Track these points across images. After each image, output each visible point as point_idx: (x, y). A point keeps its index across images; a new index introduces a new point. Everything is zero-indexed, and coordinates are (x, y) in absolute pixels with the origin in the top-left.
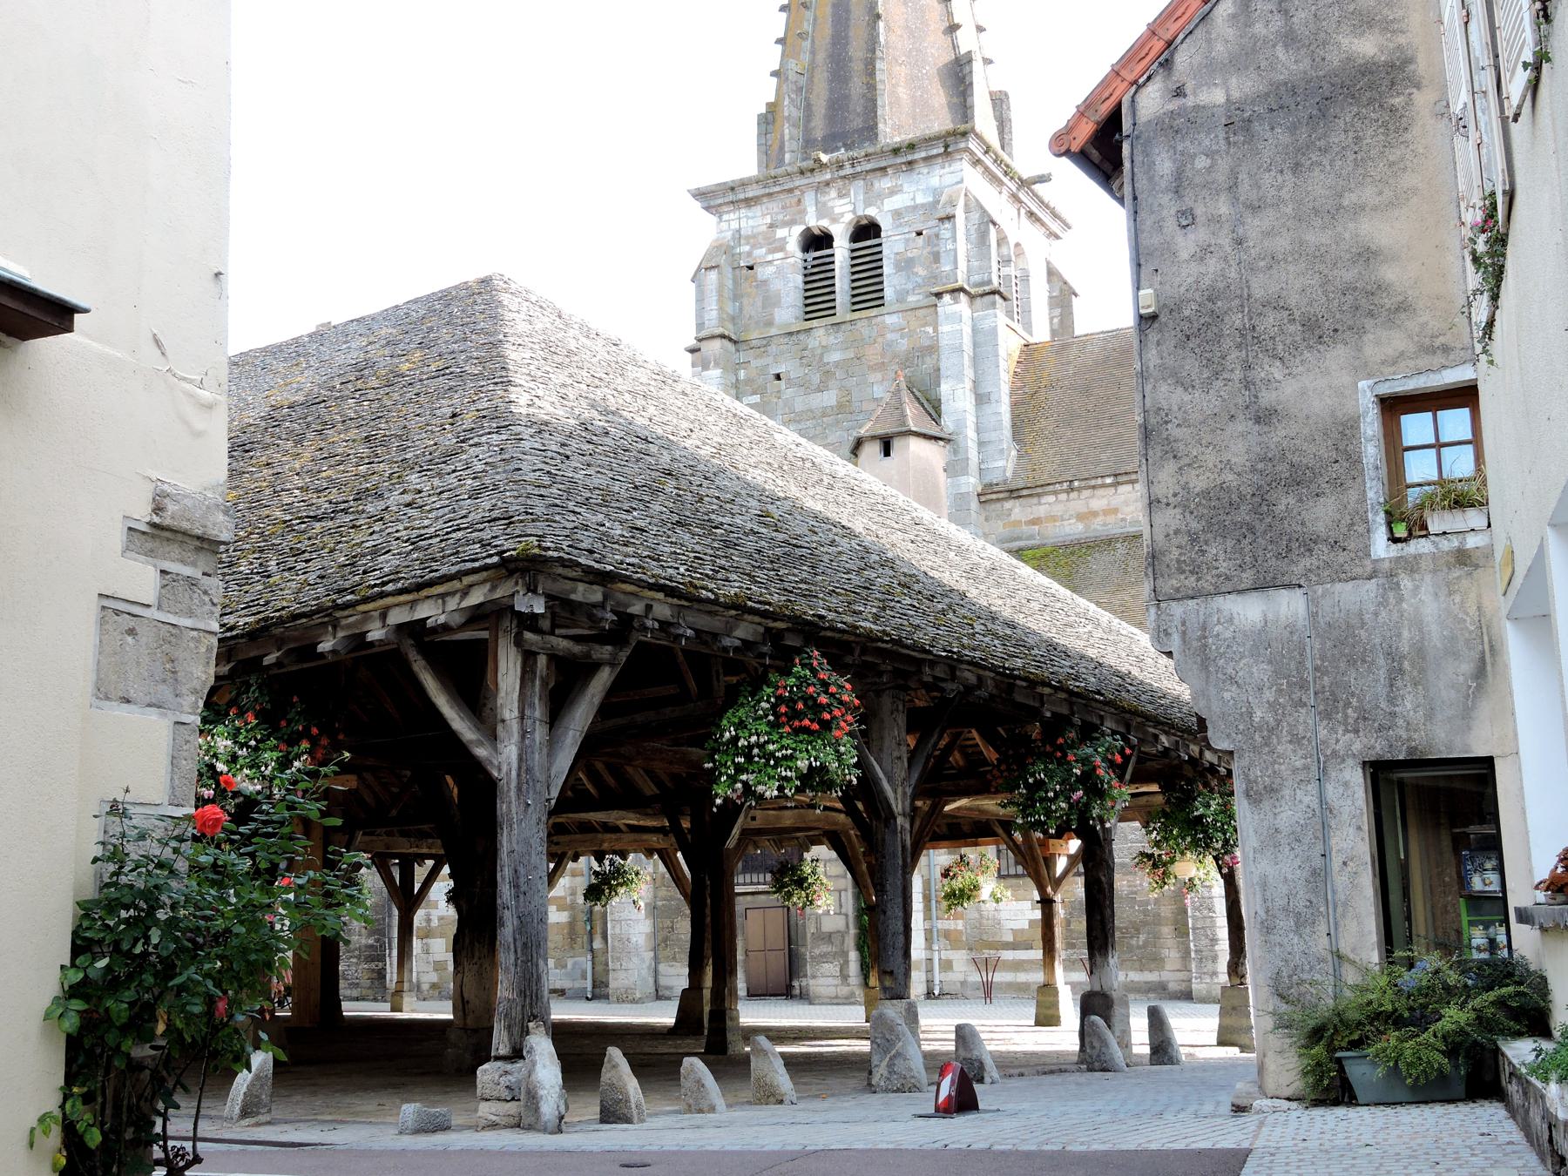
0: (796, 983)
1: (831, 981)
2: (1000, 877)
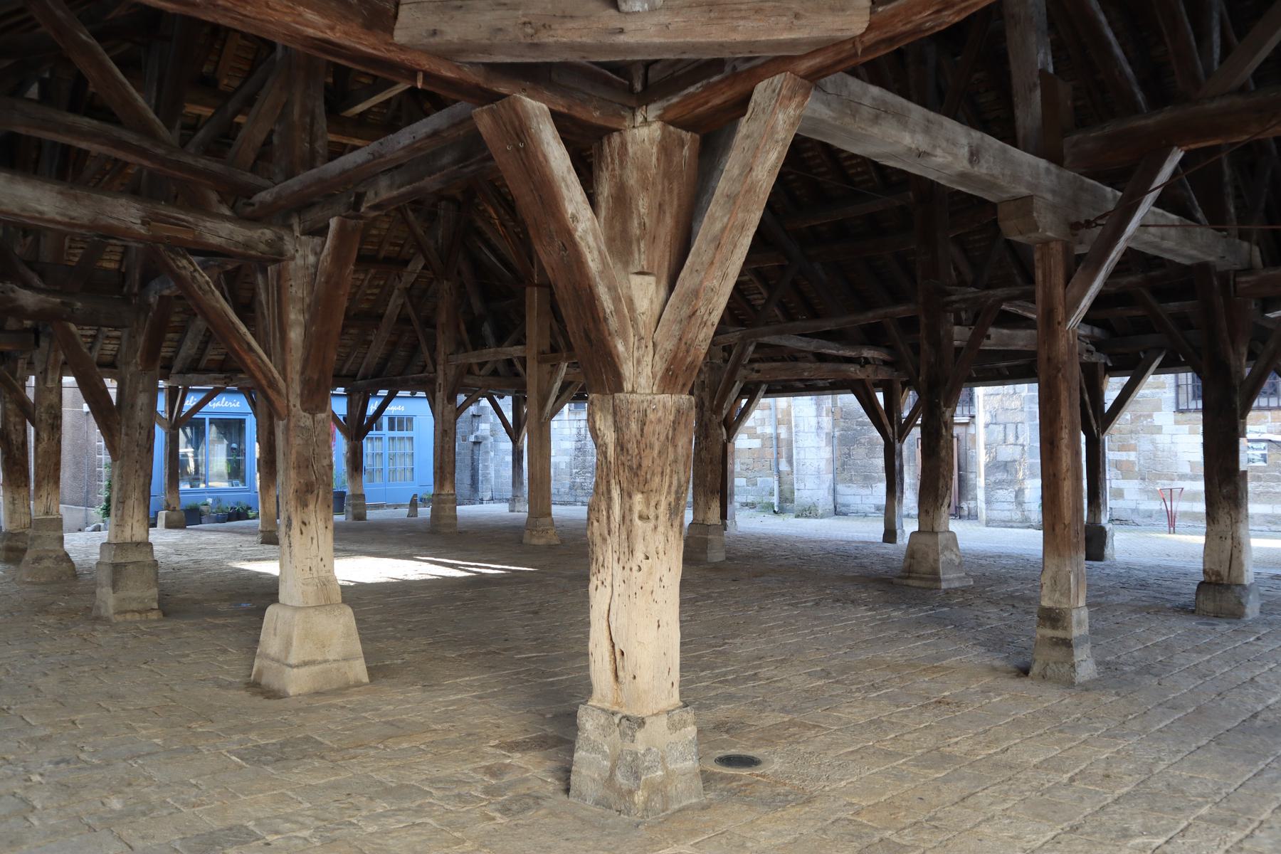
0: (964, 505)
1: (1006, 506)
2: (1179, 411)
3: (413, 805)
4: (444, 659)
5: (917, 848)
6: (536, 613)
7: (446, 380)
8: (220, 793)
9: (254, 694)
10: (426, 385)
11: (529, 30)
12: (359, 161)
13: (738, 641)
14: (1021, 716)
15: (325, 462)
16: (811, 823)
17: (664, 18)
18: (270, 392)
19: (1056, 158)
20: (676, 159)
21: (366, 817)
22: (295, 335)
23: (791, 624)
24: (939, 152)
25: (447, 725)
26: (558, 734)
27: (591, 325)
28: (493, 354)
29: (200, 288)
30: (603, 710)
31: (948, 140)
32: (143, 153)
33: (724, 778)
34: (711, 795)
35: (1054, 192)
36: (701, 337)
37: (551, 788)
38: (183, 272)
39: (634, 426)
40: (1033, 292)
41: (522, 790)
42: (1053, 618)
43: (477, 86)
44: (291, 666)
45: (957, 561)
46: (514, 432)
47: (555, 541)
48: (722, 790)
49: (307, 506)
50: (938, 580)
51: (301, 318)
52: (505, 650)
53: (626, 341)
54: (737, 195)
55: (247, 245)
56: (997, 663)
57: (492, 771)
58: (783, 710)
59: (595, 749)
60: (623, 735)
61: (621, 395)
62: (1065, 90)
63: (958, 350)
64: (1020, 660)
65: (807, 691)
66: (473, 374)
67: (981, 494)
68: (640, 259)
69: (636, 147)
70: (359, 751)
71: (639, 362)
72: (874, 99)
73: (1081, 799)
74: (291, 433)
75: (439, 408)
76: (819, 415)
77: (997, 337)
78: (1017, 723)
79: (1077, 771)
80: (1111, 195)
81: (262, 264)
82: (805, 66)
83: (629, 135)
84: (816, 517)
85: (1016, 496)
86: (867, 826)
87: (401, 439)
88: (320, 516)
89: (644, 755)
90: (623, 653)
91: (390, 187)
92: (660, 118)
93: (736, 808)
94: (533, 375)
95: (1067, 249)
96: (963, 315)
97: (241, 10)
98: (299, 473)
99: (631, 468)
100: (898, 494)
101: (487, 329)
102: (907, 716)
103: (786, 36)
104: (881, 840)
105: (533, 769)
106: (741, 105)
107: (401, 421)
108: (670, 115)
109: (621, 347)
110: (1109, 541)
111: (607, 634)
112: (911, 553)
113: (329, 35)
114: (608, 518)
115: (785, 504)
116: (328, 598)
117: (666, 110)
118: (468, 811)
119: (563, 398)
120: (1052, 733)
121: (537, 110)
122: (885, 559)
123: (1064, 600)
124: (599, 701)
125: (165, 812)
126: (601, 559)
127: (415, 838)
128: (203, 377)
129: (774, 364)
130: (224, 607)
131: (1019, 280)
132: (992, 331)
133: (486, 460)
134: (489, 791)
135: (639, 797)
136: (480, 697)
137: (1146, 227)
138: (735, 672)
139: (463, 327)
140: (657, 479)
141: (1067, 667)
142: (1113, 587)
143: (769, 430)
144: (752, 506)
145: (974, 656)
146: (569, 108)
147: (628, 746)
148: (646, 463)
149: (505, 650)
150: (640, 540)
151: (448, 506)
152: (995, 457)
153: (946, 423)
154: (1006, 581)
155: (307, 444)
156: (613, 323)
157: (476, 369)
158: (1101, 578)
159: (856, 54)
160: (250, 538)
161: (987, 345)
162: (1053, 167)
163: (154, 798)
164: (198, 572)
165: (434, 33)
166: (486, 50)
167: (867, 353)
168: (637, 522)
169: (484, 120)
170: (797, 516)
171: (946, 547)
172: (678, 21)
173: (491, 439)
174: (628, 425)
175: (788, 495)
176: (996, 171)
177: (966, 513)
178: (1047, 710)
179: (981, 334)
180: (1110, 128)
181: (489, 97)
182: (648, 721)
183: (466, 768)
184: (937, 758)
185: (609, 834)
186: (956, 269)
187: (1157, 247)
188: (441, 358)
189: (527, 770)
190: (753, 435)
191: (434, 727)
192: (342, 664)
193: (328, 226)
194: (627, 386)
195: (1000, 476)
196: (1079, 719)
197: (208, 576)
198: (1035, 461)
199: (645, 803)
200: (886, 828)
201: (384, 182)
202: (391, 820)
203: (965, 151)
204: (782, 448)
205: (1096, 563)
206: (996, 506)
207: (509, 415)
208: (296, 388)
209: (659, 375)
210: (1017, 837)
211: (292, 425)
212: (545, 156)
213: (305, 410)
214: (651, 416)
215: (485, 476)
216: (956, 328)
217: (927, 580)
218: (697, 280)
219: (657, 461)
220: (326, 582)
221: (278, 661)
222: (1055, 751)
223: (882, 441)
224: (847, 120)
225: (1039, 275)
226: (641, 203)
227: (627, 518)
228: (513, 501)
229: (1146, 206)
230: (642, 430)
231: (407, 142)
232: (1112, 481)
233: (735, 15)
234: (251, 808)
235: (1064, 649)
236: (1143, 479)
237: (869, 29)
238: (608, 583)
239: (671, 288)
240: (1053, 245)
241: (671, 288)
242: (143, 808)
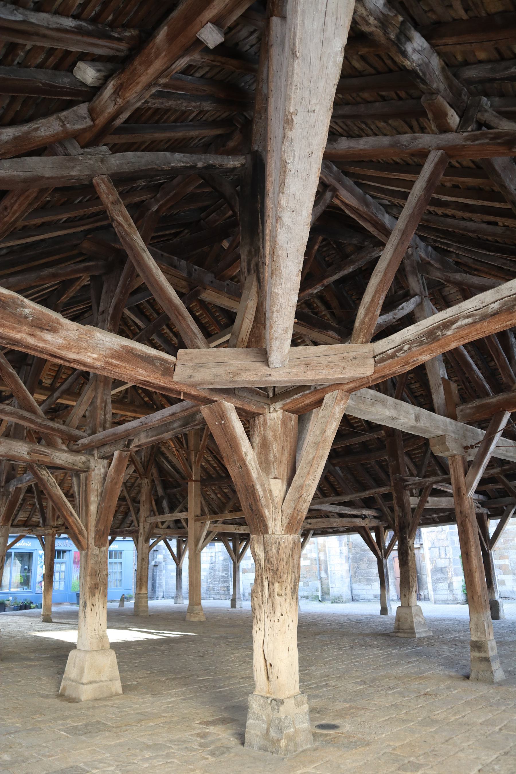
0: (421, 593)
3: (164, 753)
4: (159, 681)
5: (428, 765)
6: (202, 656)
7: (144, 531)
8: (60, 750)
9: (62, 701)
10: (134, 534)
11: (231, 375)
12: (135, 426)
13: (314, 668)
14: (469, 699)
15: (105, 573)
16: (371, 755)
17: (288, 370)
18: (79, 536)
19: (454, 417)
20: (289, 426)
21: (141, 760)
22: (93, 508)
23: (340, 658)
24: (401, 417)
25: (170, 714)
26: (234, 714)
27: (253, 503)
28: (169, 517)
29: (50, 484)
30: (262, 696)
31: (405, 412)
32: (31, 421)
33: (322, 735)
34: (317, 744)
35: (454, 432)
36: (304, 507)
37: (234, 743)
38: (43, 477)
39: (274, 550)
40: (449, 479)
41: (219, 744)
42: (478, 646)
43: (206, 398)
44: (83, 684)
45: (423, 622)
46: (178, 559)
47: (203, 619)
48: (322, 741)
49: (95, 596)
50: (413, 633)
51: (96, 499)
52: (191, 676)
53: (269, 509)
54: (319, 443)
55: (73, 464)
56: (452, 674)
57: (203, 736)
58: (345, 701)
59: (258, 718)
60: (273, 709)
61: (267, 536)
62: (454, 387)
63: (413, 509)
64: (464, 672)
65: (355, 692)
66: (159, 528)
67: (430, 586)
68: (275, 472)
69: (271, 422)
70: (128, 727)
71: (275, 519)
72: (371, 395)
73: (507, 739)
74: (89, 558)
75: (140, 546)
76: (340, 546)
77: (432, 502)
78: (467, 703)
79: (502, 725)
80: (481, 433)
81: (77, 473)
82: (347, 387)
83: (268, 416)
84: (342, 602)
85: (449, 587)
86: (400, 756)
87: (115, 563)
88: (101, 601)
89: (284, 719)
90: (271, 665)
91: (147, 437)
92: (282, 408)
93: (331, 749)
94: (192, 528)
95: (464, 459)
96: (414, 491)
97: (115, 370)
98: (91, 578)
99: (273, 570)
100: (386, 588)
101: (165, 504)
102: (410, 702)
103: (340, 376)
104: (409, 762)
105: (223, 734)
106: (319, 403)
107: (116, 553)
108: (287, 407)
109: (267, 513)
110: (501, 608)
111: (263, 655)
112: (398, 618)
113: (148, 379)
114: (262, 596)
115: (325, 596)
116: (103, 646)
117: (284, 405)
118: (194, 755)
119: (207, 540)
120: (486, 707)
121: (229, 407)
122: (383, 624)
123: (483, 636)
124: (259, 692)
125: (34, 760)
126: (258, 617)
127: (169, 769)
128: (17, 529)
129: (318, 520)
130: (32, 656)
131: (439, 472)
132: (429, 499)
133: (160, 575)
134: (201, 745)
135: (283, 743)
136: (184, 700)
137: (500, 447)
138: (316, 683)
139: (154, 503)
140: (286, 576)
141: (489, 673)
142: (506, 633)
143: (314, 555)
144: (307, 597)
145: (439, 671)
146: (243, 405)
147: (276, 715)
148: (280, 568)
149: (191, 676)
150: (278, 606)
151: (144, 600)
152: (436, 566)
153: (410, 547)
154: (450, 632)
155: (96, 563)
156: (263, 502)
157: (160, 525)
158: (499, 629)
159: (369, 382)
160: (35, 619)
161: (427, 506)
162: (453, 421)
163: (26, 754)
164: (12, 637)
165: (191, 377)
166: (211, 383)
167: (366, 512)
168: (277, 597)
169: (205, 411)
170: (332, 603)
171: (416, 615)
172: (294, 371)
173: (164, 563)
174: (271, 550)
175: (326, 591)
176: (428, 425)
177: (423, 597)
178: (482, 696)
179: (423, 501)
180: (477, 402)
181: (211, 402)
182: (285, 701)
183: (187, 734)
184: (431, 722)
185: (269, 764)
186: (408, 468)
187: (505, 456)
188: (142, 519)
189: (219, 735)
190: (306, 559)
191: (164, 715)
192: (109, 683)
193: (113, 454)
194: (270, 531)
195: (440, 576)
196: (499, 700)
197: (19, 639)
198: (459, 566)
199: (286, 747)
200: (410, 756)
201: (143, 435)
202: (155, 761)
203: (413, 416)
204: (322, 565)
205: (496, 621)
206: (439, 592)
207: (175, 550)
208: (92, 534)
209: (285, 525)
210: (478, 758)
211: (89, 553)
212: (233, 427)
213: (96, 546)
214: (282, 545)
215: (160, 584)
216: (411, 498)
217: (408, 633)
218: (302, 481)
219: (285, 567)
220: (102, 638)
221: (76, 681)
222: (490, 716)
223: (376, 559)
224: (361, 405)
225: (452, 471)
226: (274, 446)
227: (272, 596)
228: (176, 597)
229: (498, 437)
230: (278, 552)
231: (160, 418)
232: (498, 575)
233: (318, 368)
234: (80, 755)
235: (486, 663)
236: (514, 574)
237: (374, 373)
238: (262, 629)
239: (289, 485)
240: (457, 457)
241: (289, 485)
242: (22, 759)
